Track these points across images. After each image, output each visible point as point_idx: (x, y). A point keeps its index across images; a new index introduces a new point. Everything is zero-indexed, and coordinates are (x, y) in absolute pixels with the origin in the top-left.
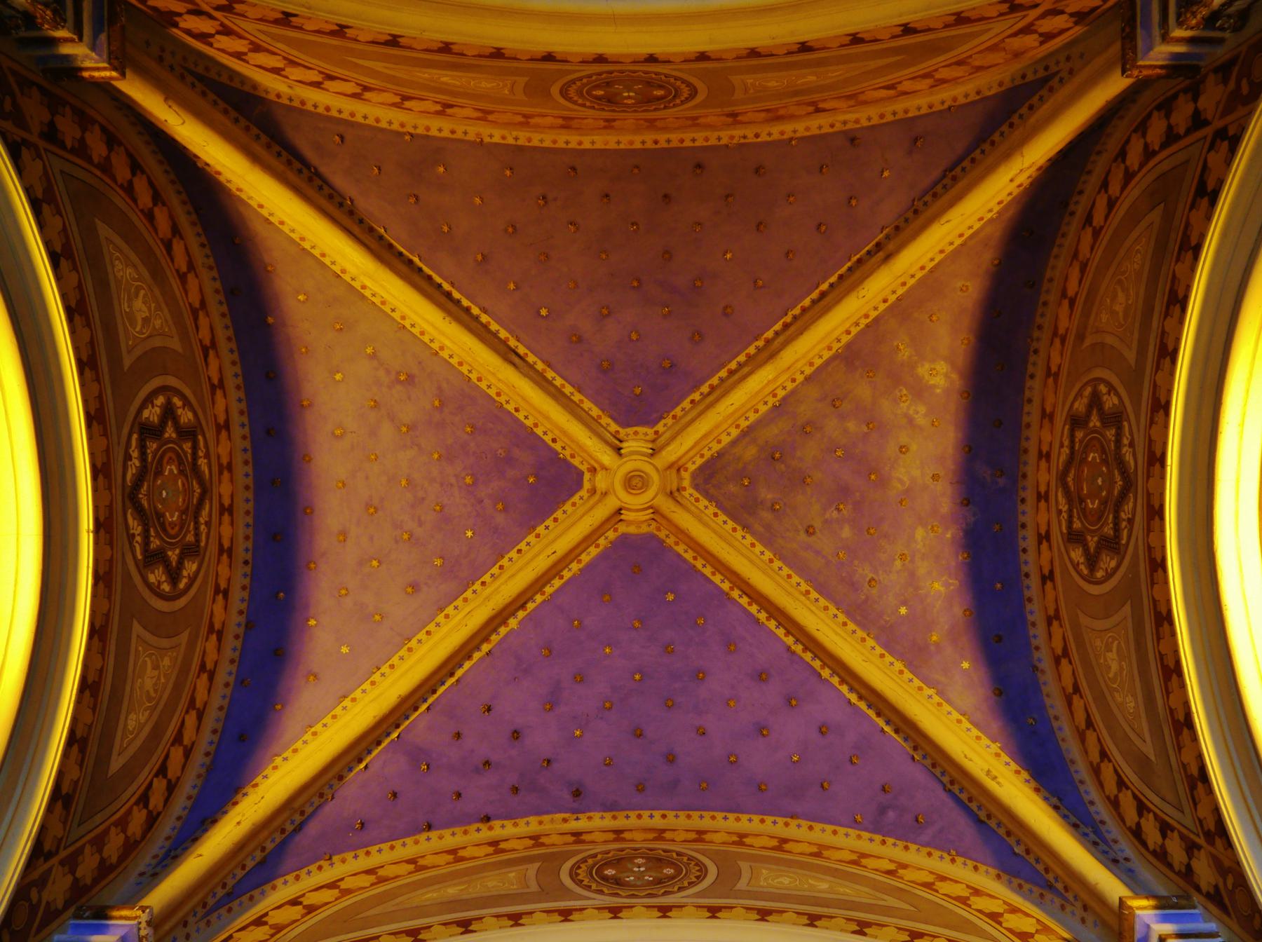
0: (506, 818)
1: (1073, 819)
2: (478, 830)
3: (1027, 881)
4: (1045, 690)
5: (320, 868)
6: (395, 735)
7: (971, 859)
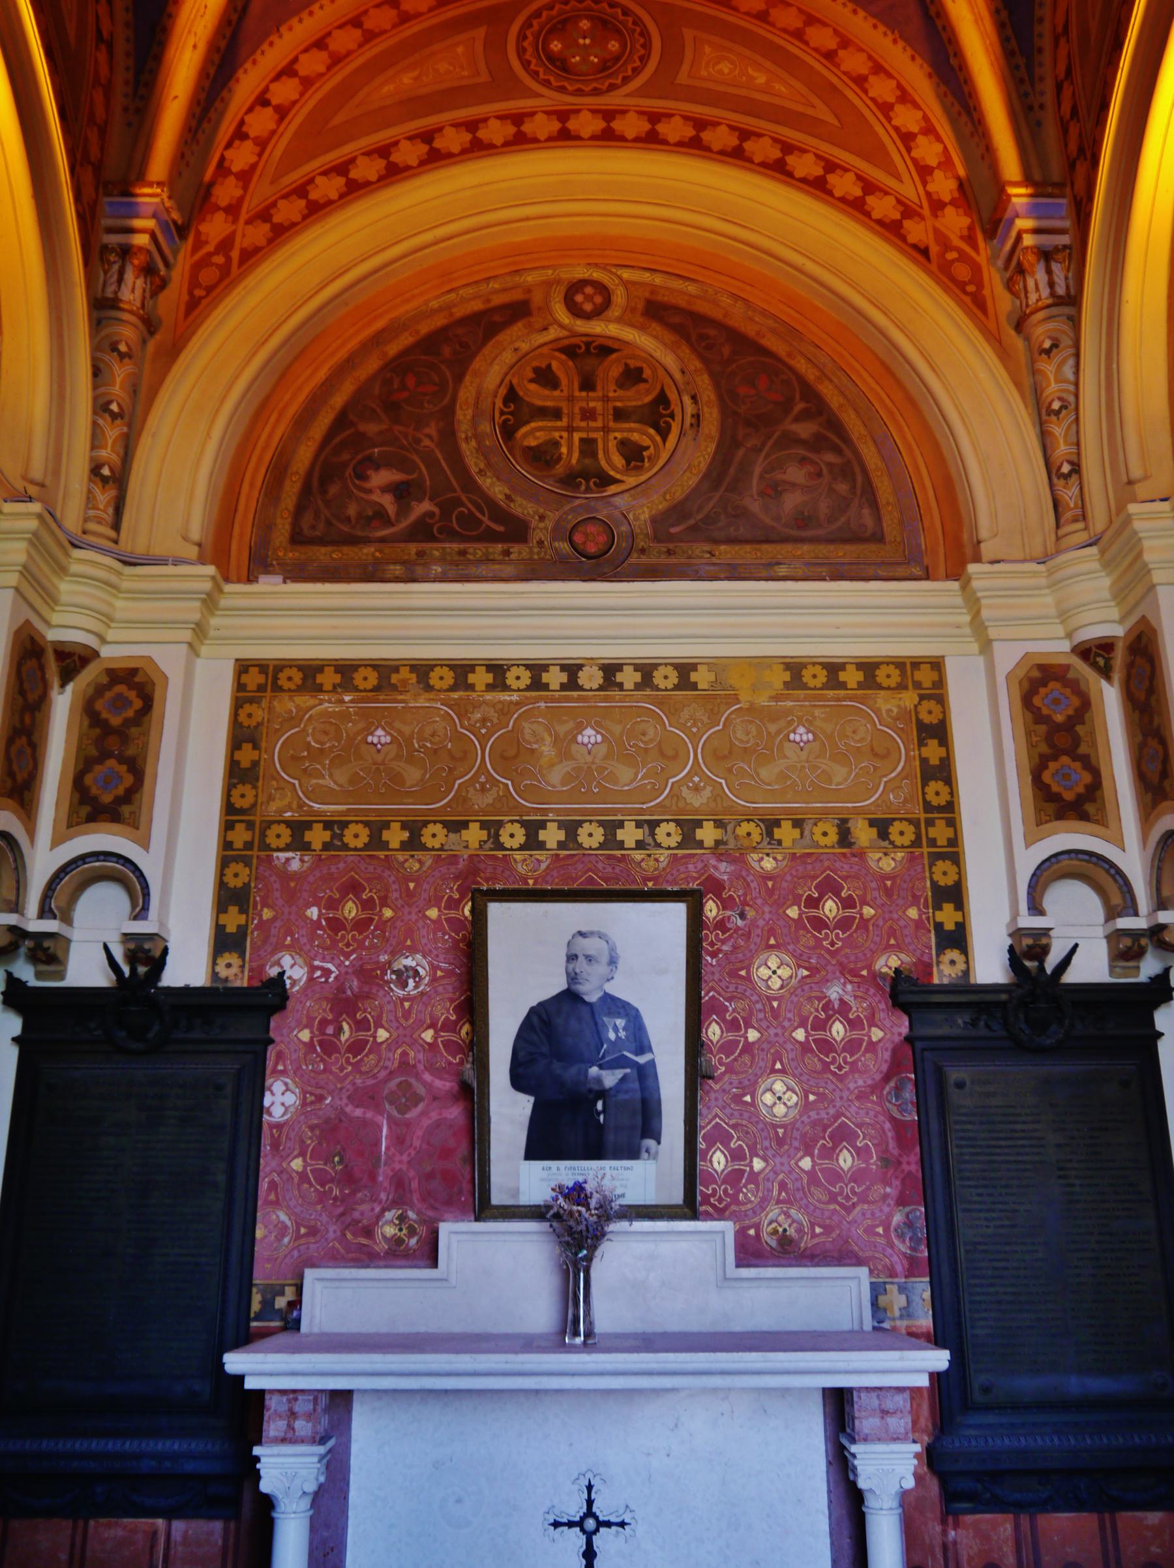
1: (1014, 44)
5: (271, 44)
7: (912, 47)
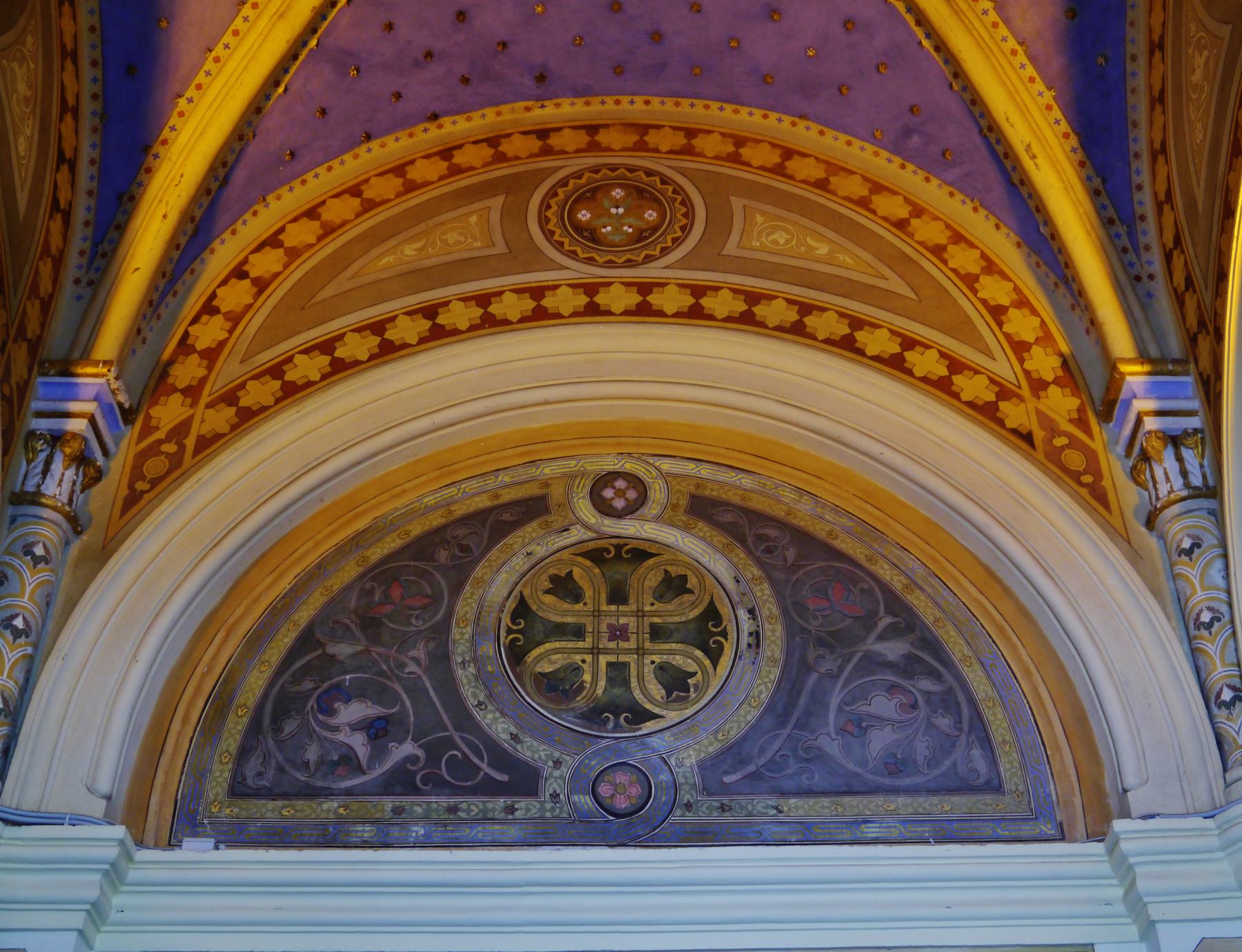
0: (458, 113)
2: (426, 130)
3: (1046, 264)
4: (1131, 15)
6: (313, 43)
7: (994, 214)
